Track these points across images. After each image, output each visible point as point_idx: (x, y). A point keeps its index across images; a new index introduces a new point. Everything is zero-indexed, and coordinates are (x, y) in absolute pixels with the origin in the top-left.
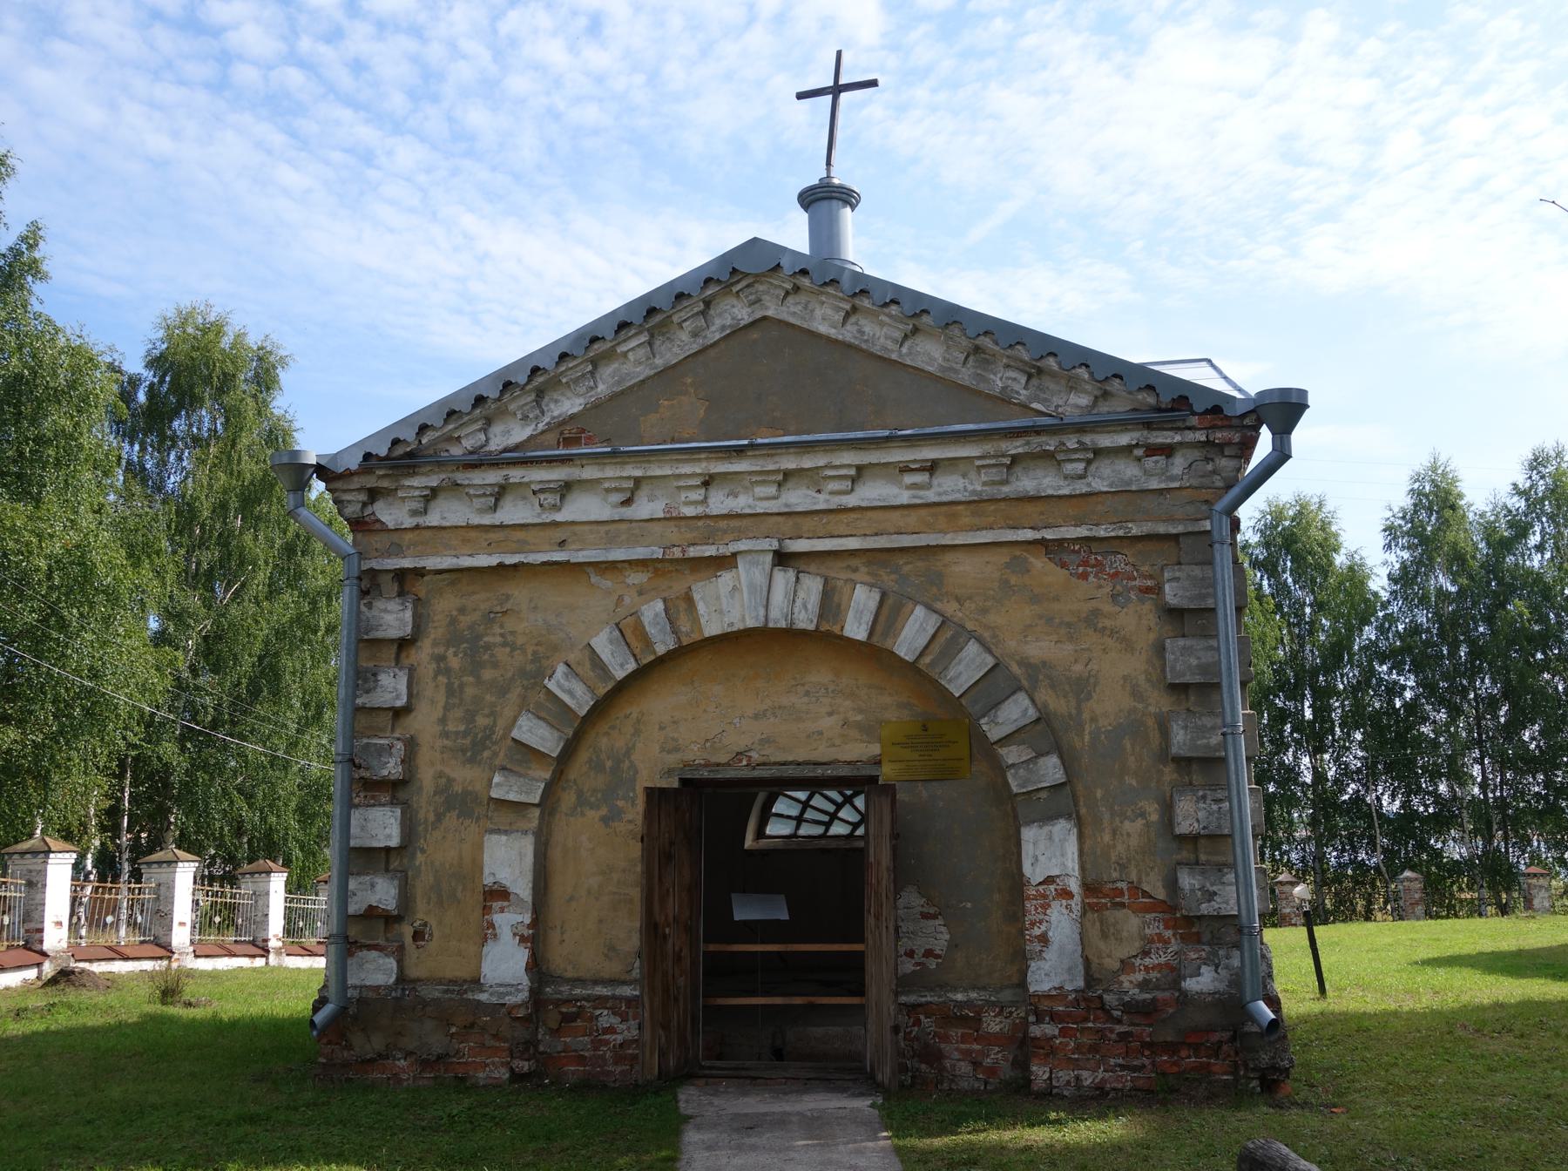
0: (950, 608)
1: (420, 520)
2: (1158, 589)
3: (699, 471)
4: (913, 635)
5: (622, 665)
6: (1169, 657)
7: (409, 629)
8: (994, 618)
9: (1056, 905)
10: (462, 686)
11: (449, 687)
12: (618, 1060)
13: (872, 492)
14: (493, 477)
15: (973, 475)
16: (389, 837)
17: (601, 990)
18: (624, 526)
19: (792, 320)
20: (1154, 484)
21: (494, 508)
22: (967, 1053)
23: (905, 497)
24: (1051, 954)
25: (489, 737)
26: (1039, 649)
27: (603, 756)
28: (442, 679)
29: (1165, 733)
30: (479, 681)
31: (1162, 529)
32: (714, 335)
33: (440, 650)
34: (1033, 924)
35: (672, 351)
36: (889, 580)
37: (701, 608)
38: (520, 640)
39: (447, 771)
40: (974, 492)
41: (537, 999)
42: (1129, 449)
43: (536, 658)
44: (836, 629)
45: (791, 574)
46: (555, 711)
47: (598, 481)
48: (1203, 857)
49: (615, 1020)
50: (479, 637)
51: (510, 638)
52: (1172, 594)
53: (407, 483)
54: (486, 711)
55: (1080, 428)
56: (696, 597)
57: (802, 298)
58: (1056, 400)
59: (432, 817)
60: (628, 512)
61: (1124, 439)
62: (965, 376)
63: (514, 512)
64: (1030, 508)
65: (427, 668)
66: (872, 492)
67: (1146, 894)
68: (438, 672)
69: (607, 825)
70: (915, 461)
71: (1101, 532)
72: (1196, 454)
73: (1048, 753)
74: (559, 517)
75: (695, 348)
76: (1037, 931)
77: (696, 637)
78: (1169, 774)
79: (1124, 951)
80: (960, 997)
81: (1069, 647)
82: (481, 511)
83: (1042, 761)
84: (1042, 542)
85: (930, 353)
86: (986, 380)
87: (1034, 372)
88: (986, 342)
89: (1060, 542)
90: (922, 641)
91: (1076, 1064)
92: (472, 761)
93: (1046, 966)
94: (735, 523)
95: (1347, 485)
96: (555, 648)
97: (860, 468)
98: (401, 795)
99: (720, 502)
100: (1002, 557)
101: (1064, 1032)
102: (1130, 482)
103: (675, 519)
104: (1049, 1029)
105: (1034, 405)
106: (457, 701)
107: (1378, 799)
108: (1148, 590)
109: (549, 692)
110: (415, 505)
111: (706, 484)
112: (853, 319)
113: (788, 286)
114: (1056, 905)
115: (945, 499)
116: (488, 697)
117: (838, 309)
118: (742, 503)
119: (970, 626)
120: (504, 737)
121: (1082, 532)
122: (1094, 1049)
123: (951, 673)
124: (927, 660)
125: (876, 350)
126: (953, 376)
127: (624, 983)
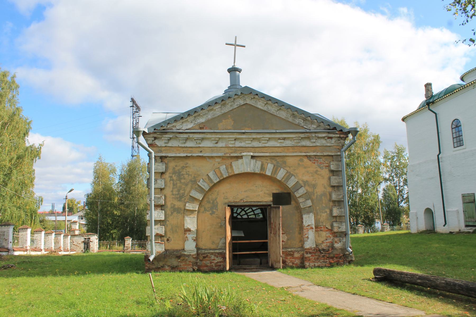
0: (288, 169)
2: (329, 166)
4: (280, 175)
6: (332, 180)
7: (164, 170)
9: (310, 230)
10: (176, 184)
12: (216, 266)
13: (271, 143)
14: (186, 136)
15: (293, 141)
17: (211, 251)
18: (215, 148)
19: (253, 104)
20: (329, 145)
21: (185, 143)
22: (291, 261)
23: (278, 145)
24: (309, 240)
26: (305, 178)
28: (172, 182)
29: (330, 195)
30: (181, 182)
31: (330, 154)
32: (235, 106)
33: (171, 175)
35: (227, 109)
36: (275, 162)
37: (234, 167)
38: (190, 173)
41: (198, 254)
42: (324, 137)
43: (194, 177)
44: (264, 173)
45: (255, 160)
46: (201, 190)
47: (211, 138)
48: (338, 220)
50: (180, 172)
51: (188, 173)
52: (333, 167)
53: (164, 136)
55: (316, 133)
56: (233, 165)
57: (255, 100)
59: (170, 213)
60: (216, 145)
61: (324, 135)
62: (290, 119)
63: (189, 144)
64: (304, 148)
65: (168, 179)
66: (271, 143)
67: (327, 228)
68: (170, 180)
71: (318, 154)
72: (336, 139)
73: (308, 200)
74: (200, 146)
75: (231, 109)
76: (306, 236)
77: (232, 174)
78: (331, 204)
79: (322, 239)
80: (290, 250)
81: (312, 178)
82: (182, 143)
84: (306, 156)
85: (283, 114)
87: (305, 120)
88: (296, 113)
89: (310, 156)
90: (282, 176)
91: (314, 262)
92: (180, 201)
93: (308, 243)
94: (241, 149)
96: (199, 175)
97: (269, 138)
98: (163, 208)
99: (238, 144)
100: (298, 159)
101: (312, 256)
104: (309, 255)
108: (327, 166)
109: (198, 185)
111: (235, 140)
113: (253, 97)
114: (310, 230)
117: (263, 103)
118: (243, 144)
119: (292, 173)
120: (187, 195)
121: (315, 154)
122: (318, 259)
123: (289, 183)
124: (283, 180)
125: (271, 112)
126: (288, 119)
127: (216, 249)
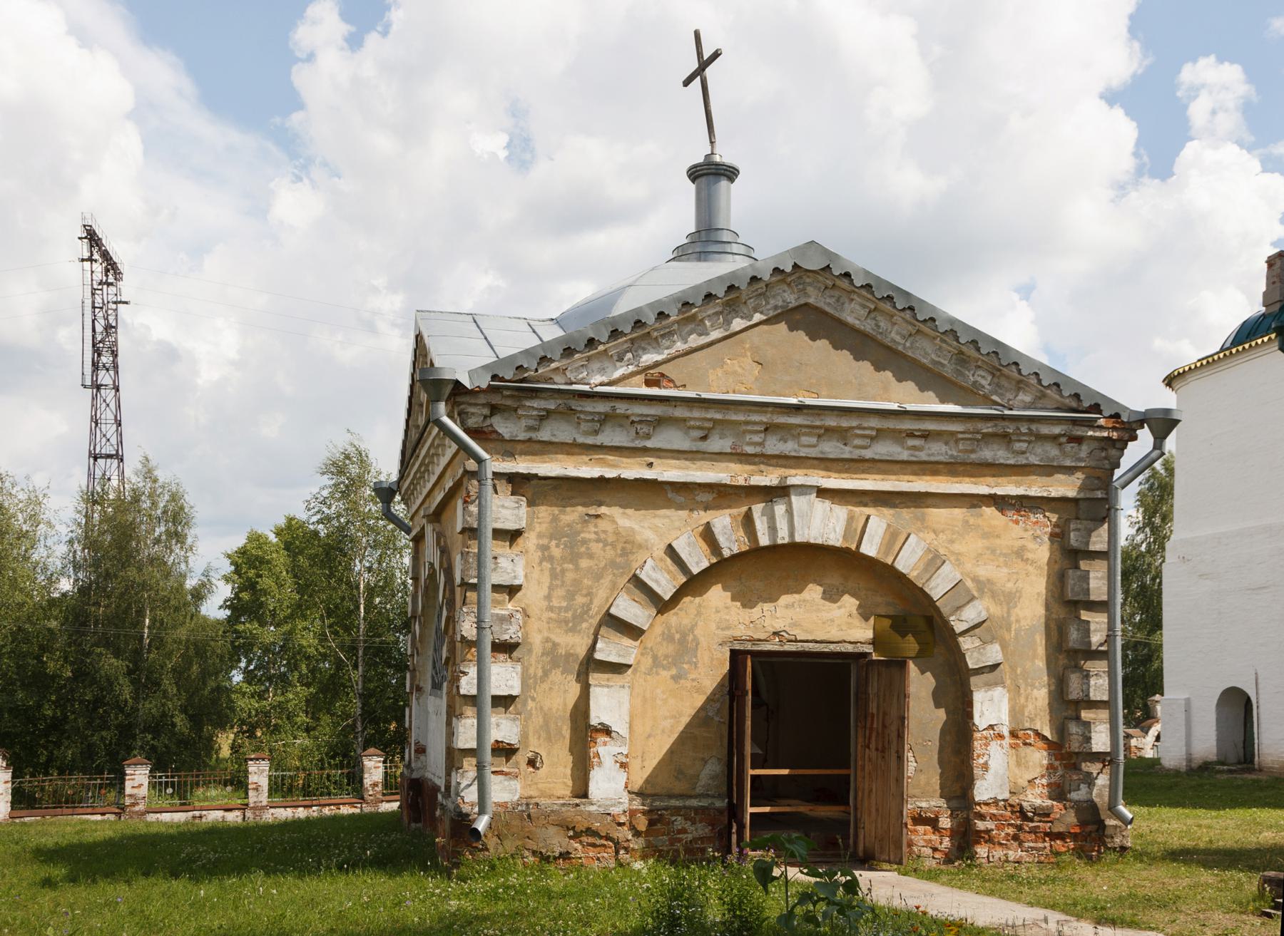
1: (534, 435)
3: (765, 420)
5: (697, 563)
8: (957, 547)
10: (563, 571)
11: (552, 570)
15: (952, 443)
16: (512, 687)
17: (674, 803)
20: (1068, 463)
23: (905, 455)
25: (587, 612)
27: (673, 631)
28: (547, 565)
30: (577, 568)
33: (545, 541)
34: (979, 756)
39: (553, 637)
40: (952, 456)
42: (1054, 438)
47: (684, 420)
49: (688, 825)
51: (603, 536)
53: (528, 404)
54: (584, 592)
57: (836, 293)
58: (1009, 395)
59: (540, 673)
61: (1057, 430)
69: (676, 682)
70: (919, 430)
72: (1095, 445)
76: (981, 761)
81: (1005, 570)
82: (586, 433)
83: (989, 647)
86: (962, 374)
87: (996, 372)
92: (573, 630)
95: (720, 585)
102: (1053, 459)
103: (737, 454)
105: (995, 398)
106: (559, 582)
107: (364, 729)
110: (531, 422)
112: (872, 315)
113: (830, 283)
115: (932, 459)
116: (585, 581)
117: (864, 306)
125: (887, 341)
127: (691, 797)
